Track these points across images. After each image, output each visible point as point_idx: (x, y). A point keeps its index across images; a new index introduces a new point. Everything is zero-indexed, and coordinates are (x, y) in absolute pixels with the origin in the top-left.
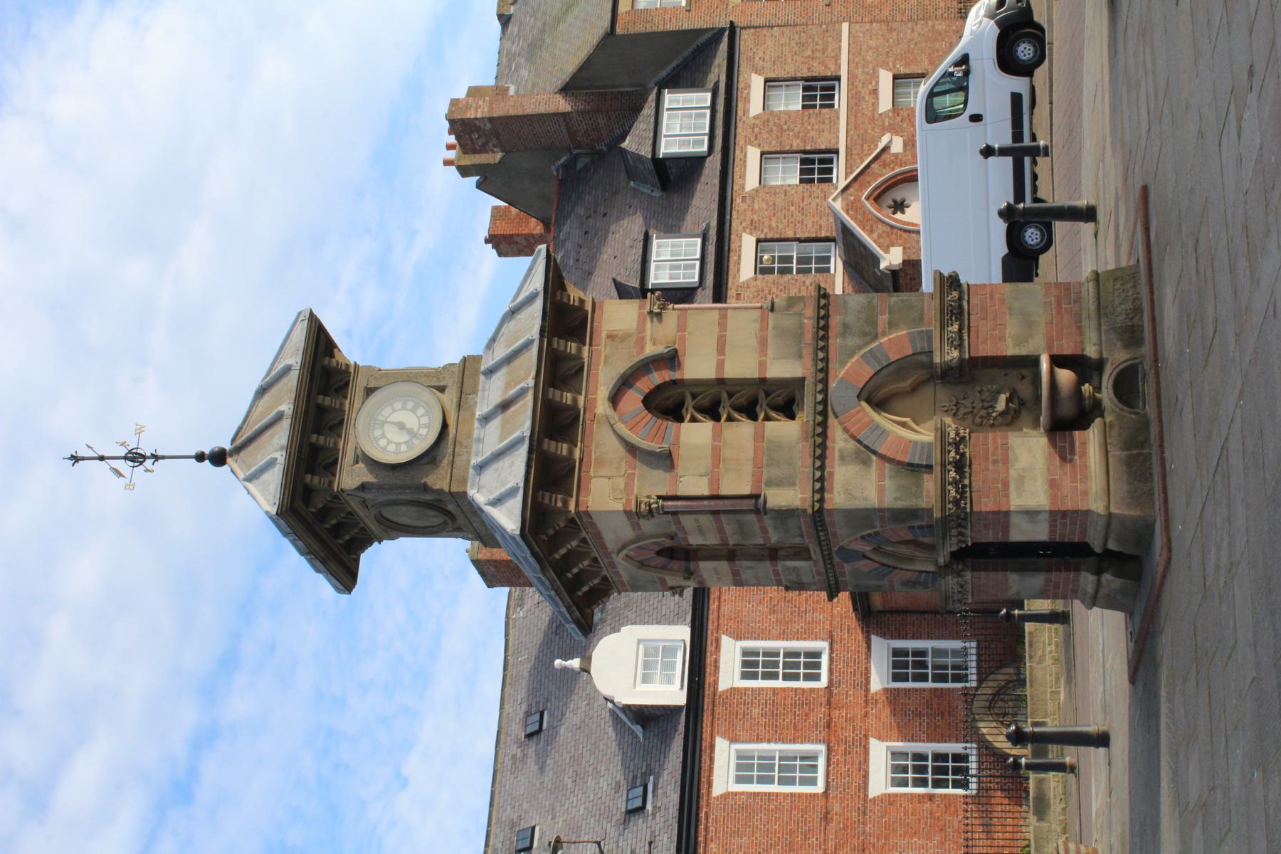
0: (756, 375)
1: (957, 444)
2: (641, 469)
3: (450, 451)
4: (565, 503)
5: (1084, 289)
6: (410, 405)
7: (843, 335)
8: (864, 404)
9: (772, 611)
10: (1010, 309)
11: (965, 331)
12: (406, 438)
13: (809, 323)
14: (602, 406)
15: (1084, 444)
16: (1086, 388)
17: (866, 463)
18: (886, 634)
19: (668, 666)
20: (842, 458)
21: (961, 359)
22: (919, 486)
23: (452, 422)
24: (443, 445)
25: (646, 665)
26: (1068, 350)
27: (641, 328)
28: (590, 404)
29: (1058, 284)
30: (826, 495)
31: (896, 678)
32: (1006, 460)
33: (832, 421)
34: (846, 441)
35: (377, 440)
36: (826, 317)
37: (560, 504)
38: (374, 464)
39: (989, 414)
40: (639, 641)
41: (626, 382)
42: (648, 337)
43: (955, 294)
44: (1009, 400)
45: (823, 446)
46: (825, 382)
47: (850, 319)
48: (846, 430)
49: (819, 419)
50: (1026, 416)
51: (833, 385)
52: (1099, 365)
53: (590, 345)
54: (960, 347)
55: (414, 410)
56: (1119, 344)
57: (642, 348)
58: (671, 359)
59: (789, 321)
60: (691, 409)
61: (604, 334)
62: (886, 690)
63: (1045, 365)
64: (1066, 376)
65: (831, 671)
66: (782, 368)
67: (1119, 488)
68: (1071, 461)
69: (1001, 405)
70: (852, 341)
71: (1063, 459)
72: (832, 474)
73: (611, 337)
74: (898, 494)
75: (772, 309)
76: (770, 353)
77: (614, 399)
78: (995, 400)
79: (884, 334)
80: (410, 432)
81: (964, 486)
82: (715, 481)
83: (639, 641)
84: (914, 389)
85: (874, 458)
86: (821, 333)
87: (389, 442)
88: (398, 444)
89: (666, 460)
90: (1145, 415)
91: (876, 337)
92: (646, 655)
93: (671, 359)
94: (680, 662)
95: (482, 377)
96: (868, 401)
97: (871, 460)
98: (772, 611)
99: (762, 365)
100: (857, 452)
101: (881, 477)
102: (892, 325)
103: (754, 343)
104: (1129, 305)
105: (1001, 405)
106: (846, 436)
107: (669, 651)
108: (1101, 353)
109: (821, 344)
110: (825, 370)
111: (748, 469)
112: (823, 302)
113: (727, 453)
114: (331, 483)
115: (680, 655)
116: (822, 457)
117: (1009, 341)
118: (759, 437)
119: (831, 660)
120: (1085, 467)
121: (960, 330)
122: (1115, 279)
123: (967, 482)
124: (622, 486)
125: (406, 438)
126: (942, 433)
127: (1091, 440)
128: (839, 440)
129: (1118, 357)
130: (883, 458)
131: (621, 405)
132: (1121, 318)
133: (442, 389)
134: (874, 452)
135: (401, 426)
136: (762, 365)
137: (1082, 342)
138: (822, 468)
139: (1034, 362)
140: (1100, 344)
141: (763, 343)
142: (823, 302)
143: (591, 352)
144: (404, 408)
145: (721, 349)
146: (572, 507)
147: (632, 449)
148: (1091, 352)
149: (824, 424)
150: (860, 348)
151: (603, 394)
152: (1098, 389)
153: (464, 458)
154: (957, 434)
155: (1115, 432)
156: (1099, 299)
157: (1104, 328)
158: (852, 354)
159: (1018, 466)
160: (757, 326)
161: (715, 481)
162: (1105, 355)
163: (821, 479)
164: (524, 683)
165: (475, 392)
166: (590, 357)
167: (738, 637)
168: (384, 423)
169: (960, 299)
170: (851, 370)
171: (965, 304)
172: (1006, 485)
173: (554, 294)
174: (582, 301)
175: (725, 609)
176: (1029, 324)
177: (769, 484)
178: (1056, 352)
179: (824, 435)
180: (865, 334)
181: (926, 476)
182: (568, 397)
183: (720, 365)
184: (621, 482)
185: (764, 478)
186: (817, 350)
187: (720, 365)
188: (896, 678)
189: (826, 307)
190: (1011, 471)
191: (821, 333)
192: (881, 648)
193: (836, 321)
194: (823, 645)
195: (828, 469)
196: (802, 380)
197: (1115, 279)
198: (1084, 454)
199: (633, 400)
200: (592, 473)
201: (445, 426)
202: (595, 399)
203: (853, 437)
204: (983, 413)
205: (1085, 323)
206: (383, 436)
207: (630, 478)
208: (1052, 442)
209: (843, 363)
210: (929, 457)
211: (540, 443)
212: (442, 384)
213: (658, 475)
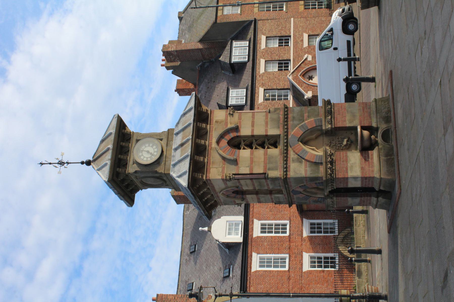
0: (264, 134)
1: (330, 156)
2: (227, 165)
3: (164, 160)
4: (202, 177)
5: (371, 104)
6: (151, 145)
7: (293, 120)
8: (300, 143)
9: (271, 211)
10: (347, 111)
11: (333, 118)
12: (150, 156)
13: (282, 117)
14: (214, 145)
15: (372, 155)
16: (373, 137)
17: (301, 162)
18: (308, 218)
19: (237, 229)
20: (293, 161)
21: (332, 128)
22: (318, 169)
23: (165, 150)
24: (162, 158)
25: (230, 229)
26: (366, 124)
27: (226, 119)
28: (210, 144)
29: (363, 103)
30: (288, 173)
31: (311, 232)
32: (347, 161)
33: (290, 149)
34: (294, 155)
35: (140, 156)
36: (287, 114)
37: (200, 177)
38: (139, 165)
39: (341, 146)
40: (227, 221)
41: (221, 137)
42: (229, 122)
43: (329, 107)
44: (347, 141)
45: (287, 157)
46: (287, 136)
47: (295, 115)
48: (294, 151)
49: (285, 148)
50: (353, 146)
51: (290, 137)
52: (377, 129)
53: (210, 124)
54: (331, 124)
55: (152, 147)
56: (383, 122)
57: (227, 125)
58: (236, 129)
59: (275, 116)
60: (243, 145)
61: (214, 121)
62: (308, 236)
63: (359, 130)
64: (366, 133)
65: (290, 230)
66: (273, 132)
67: (384, 169)
68: (368, 161)
69: (345, 143)
70: (296, 122)
71: (365, 160)
72: (290, 166)
73: (217, 122)
74: (311, 172)
75: (269, 112)
76: (269, 126)
77: (218, 142)
78: (343, 141)
79: (306, 120)
80: (151, 154)
81: (333, 169)
82: (251, 169)
83: (227, 221)
84: (317, 138)
85: (303, 160)
86: (286, 120)
87: (144, 157)
88: (147, 158)
89: (235, 162)
90: (392, 145)
91: (303, 121)
92: (229, 226)
93: (236, 129)
94: (240, 228)
95: (174, 136)
96: (301, 142)
97: (302, 161)
98: (271, 211)
99: (266, 131)
100: (298, 159)
101: (306, 167)
102: (309, 117)
103: (263, 123)
104: (386, 110)
105: (345, 143)
106: (294, 153)
107: (237, 225)
108: (377, 125)
109: (286, 123)
110: (287, 132)
111: (262, 165)
112: (286, 110)
113: (255, 159)
114: (125, 171)
115: (240, 226)
116: (286, 160)
117: (347, 122)
118: (266, 154)
119: (290, 227)
120: (373, 163)
121: (331, 118)
122: (382, 101)
123: (334, 168)
124: (221, 171)
125: (150, 156)
126: (326, 152)
127: (374, 154)
128: (292, 155)
129: (383, 127)
130: (306, 160)
131: (220, 144)
132: (384, 114)
133: (161, 140)
134: (304, 159)
135: (148, 152)
136: (266, 131)
137: (371, 122)
138: (286, 164)
139: (355, 128)
140: (377, 122)
141: (267, 123)
142: (286, 110)
143: (210, 127)
144: (149, 146)
145: (253, 126)
146: (204, 178)
147: (224, 158)
148: (374, 125)
149: (287, 150)
150: (298, 124)
151: (214, 140)
152: (377, 137)
153: (169, 162)
154: (331, 152)
155: (382, 151)
156: (376, 107)
157: (378, 117)
158: (296, 126)
159: (351, 162)
160: (264, 118)
161: (251, 169)
162: (379, 126)
163: (286, 168)
164: (189, 236)
165: (172, 140)
166: (210, 129)
167: (259, 220)
168: (142, 151)
169: (331, 108)
170: (295, 132)
171: (333, 110)
172: (347, 169)
173: (198, 108)
174: (207, 110)
175: (255, 210)
176: (354, 116)
177: (269, 169)
178: (362, 125)
179: (287, 153)
180: (300, 120)
181: (320, 166)
182: (203, 142)
183: (253, 131)
184: (221, 169)
185: (268, 167)
186: (284, 125)
187: (253, 131)
188: (311, 232)
189: (287, 111)
190: (348, 164)
191: (286, 120)
192: (306, 223)
193: (290, 116)
194: (287, 222)
195: (288, 164)
196: (280, 135)
197: (382, 101)
198: (372, 158)
199: (224, 142)
200: (211, 166)
201: (162, 152)
202: (212, 142)
203: (296, 154)
204: (339, 145)
205: (372, 115)
206: (142, 155)
207: (223, 168)
208: (362, 155)
209: (293, 130)
210: (321, 160)
211: (194, 157)
212: (161, 138)
213: (233, 167)
